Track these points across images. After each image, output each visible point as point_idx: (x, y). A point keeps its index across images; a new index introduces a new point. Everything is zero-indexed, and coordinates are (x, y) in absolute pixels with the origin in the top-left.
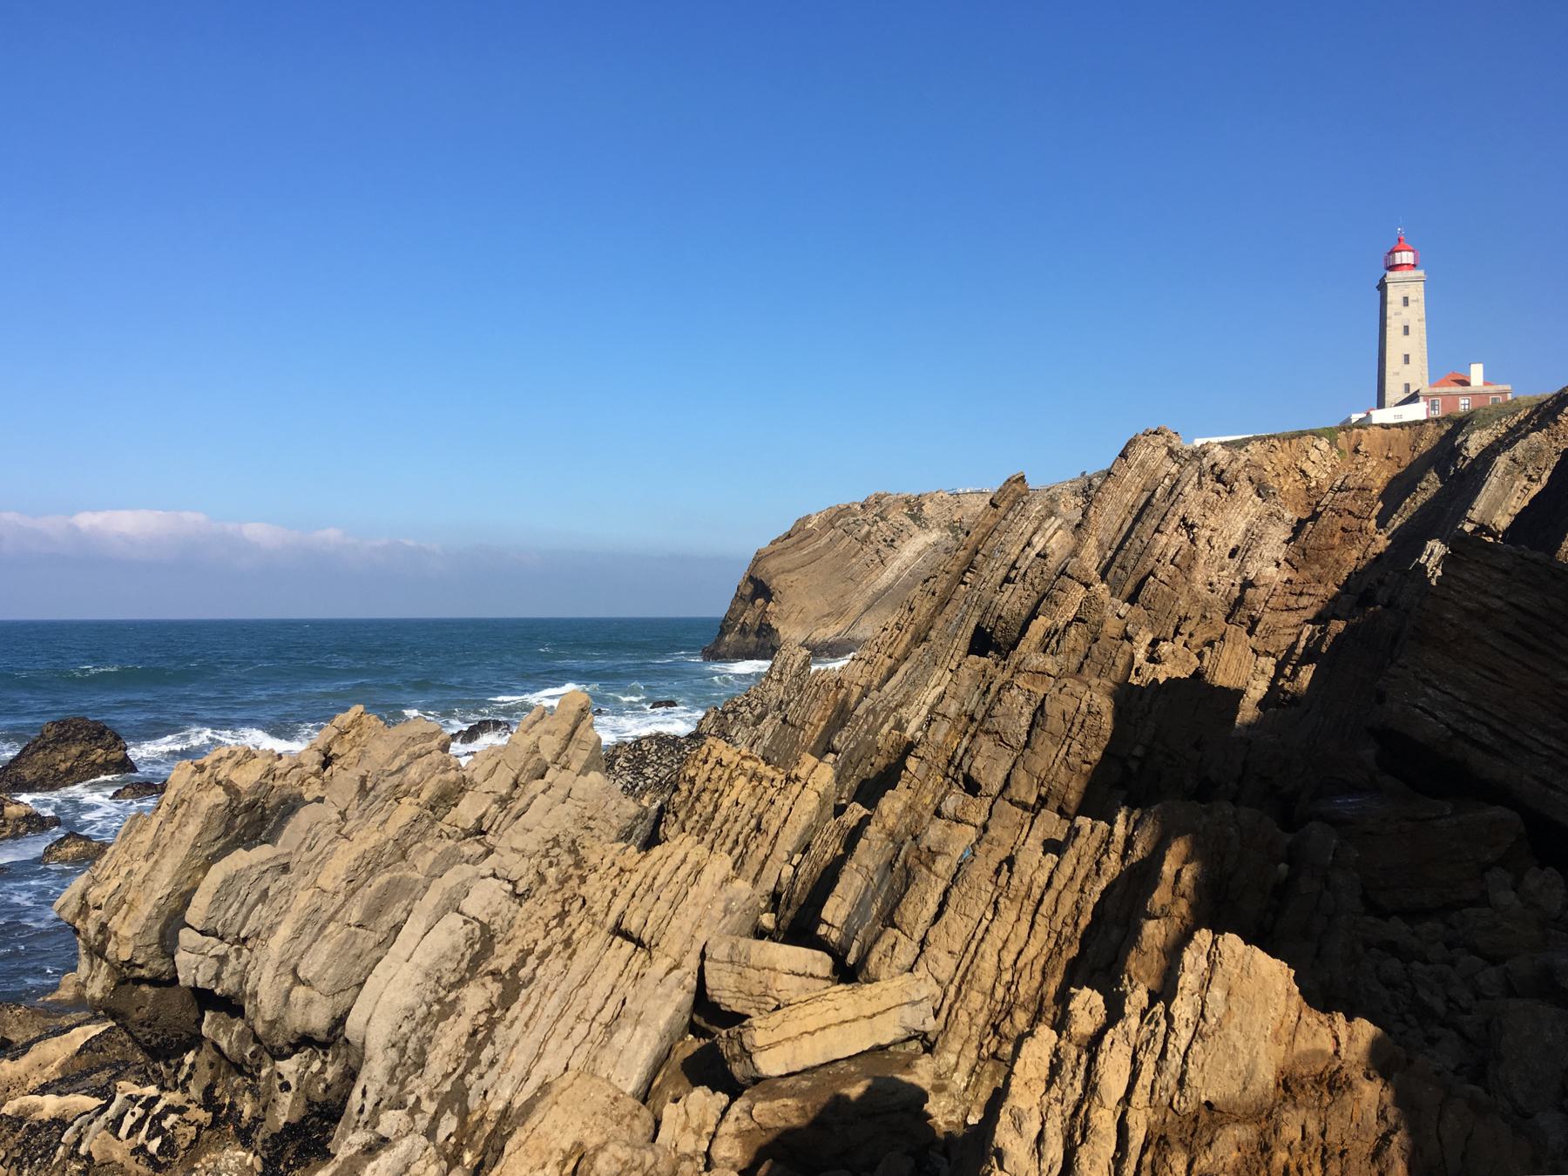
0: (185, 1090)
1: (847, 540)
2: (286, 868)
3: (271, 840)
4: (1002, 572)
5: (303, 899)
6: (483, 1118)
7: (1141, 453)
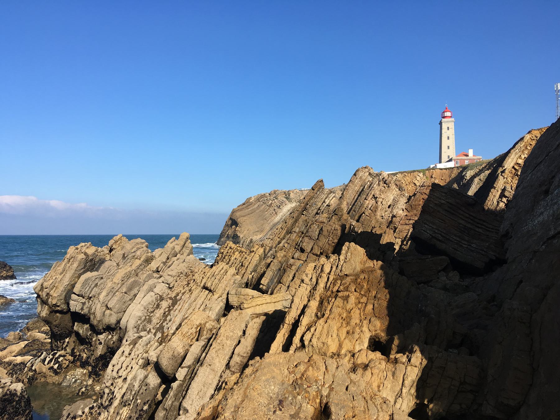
0: (66, 350)
1: (264, 206)
2: (102, 278)
3: (97, 270)
4: (316, 211)
5: (110, 284)
6: (167, 335)
7: (360, 174)
